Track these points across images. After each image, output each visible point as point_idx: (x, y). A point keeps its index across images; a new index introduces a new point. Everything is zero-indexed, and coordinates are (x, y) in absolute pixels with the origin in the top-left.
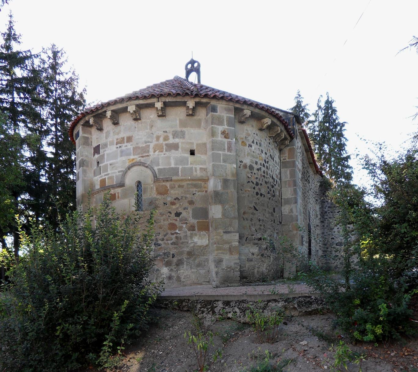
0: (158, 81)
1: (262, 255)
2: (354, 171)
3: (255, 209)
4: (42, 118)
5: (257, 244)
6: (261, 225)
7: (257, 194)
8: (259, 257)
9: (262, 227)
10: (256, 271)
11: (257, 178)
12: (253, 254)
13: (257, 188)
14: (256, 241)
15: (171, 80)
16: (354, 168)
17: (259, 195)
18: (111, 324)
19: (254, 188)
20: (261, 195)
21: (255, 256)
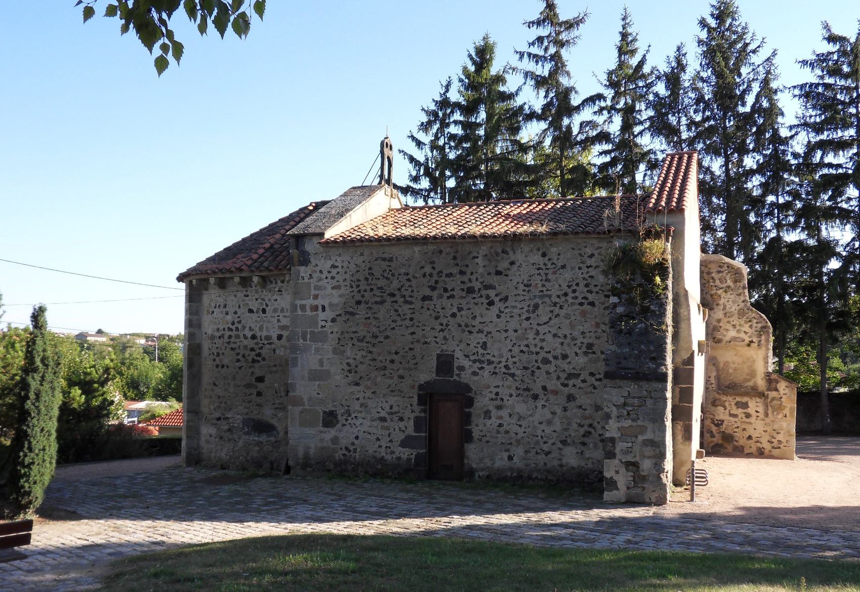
0: (202, 258)
1: (221, 438)
2: (530, 104)
3: (214, 384)
4: (83, 397)
5: (216, 424)
6: (221, 403)
7: (217, 366)
8: (217, 440)
9: (223, 405)
10: (213, 455)
11: (217, 348)
12: (211, 436)
13: (217, 359)
14: (215, 421)
15: (194, 267)
16: (527, 101)
17: (220, 368)
18: (179, 422)
19: (214, 360)
20: (223, 366)
21: (213, 438)
